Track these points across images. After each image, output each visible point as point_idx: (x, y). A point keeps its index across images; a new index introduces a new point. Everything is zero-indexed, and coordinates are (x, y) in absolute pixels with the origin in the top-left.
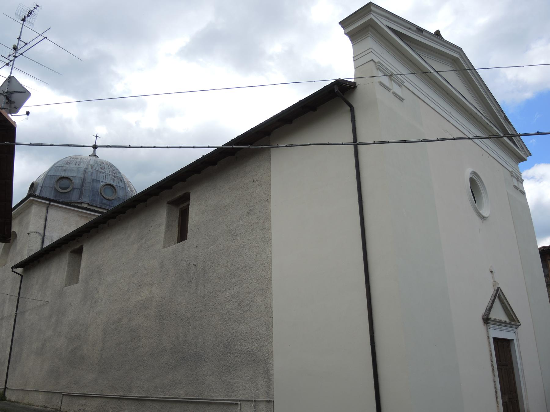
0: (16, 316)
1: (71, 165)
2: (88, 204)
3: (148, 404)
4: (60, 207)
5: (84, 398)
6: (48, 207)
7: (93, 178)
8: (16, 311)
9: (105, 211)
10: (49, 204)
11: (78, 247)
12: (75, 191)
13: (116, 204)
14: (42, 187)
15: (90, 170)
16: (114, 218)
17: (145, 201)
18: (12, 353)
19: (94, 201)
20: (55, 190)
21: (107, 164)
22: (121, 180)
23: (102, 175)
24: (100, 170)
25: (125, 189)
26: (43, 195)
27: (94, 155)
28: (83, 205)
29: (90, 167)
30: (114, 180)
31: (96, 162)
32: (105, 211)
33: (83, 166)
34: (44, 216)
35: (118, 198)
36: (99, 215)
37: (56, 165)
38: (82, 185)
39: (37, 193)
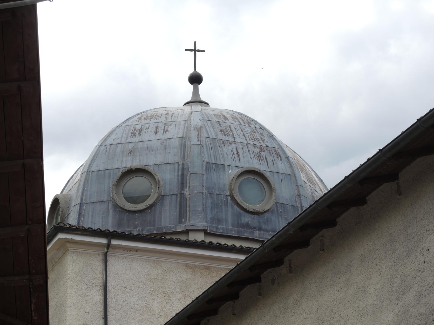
1: (145, 137)
2: (206, 233)
4: (137, 250)
6: (106, 255)
7: (206, 160)
9: (256, 246)
10: (109, 246)
12: (167, 201)
13: (280, 224)
14: (81, 204)
16: (305, 243)
17: (393, 176)
19: (219, 221)
20: (116, 206)
21: (234, 118)
22: (279, 155)
23: (228, 149)
24: (221, 136)
25: (292, 177)
26: (87, 224)
27: (196, 100)
28: (192, 237)
29: (193, 134)
30: (259, 157)
31: (206, 119)
32: (256, 246)
33: (175, 132)
35: (279, 207)
36: (242, 257)
37: (109, 142)
38: (183, 184)
39: (72, 220)
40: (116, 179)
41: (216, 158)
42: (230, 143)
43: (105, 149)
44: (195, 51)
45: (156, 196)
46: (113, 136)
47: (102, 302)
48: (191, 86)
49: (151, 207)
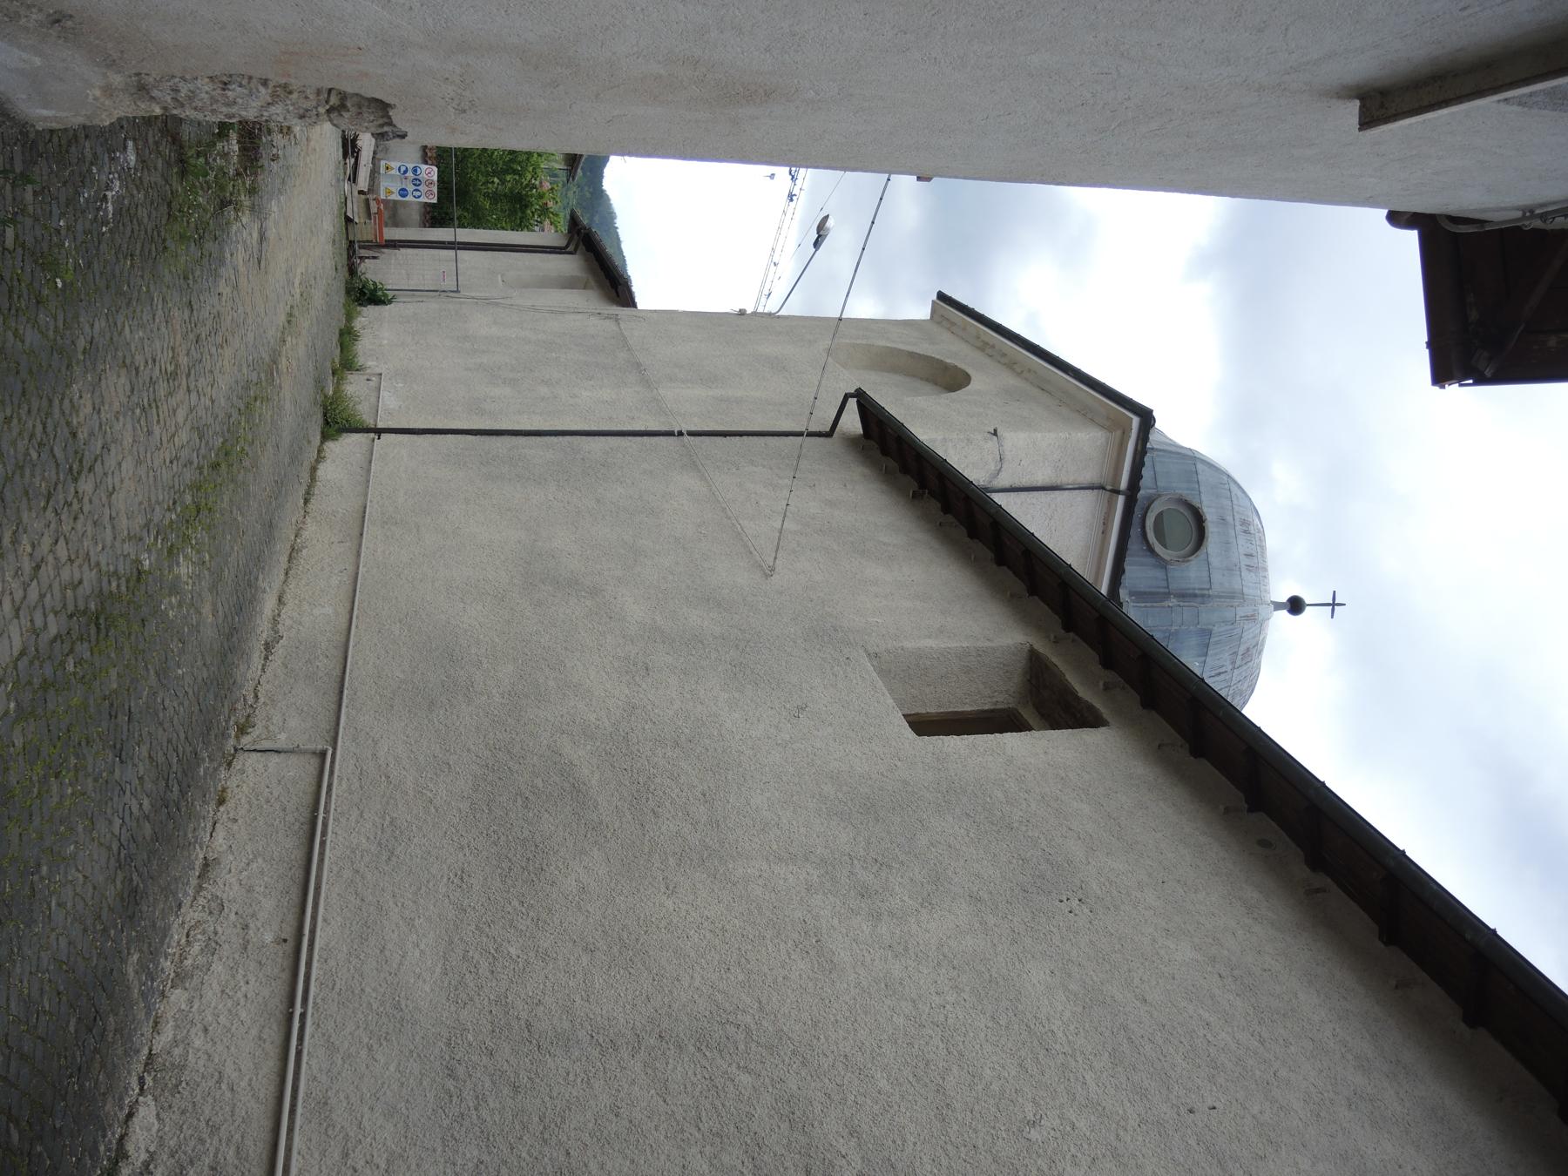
0: (670, 434)
1: (1242, 539)
3: (273, 1034)
4: (1105, 533)
5: (288, 932)
7: (1216, 629)
8: (691, 434)
10: (1117, 492)
11: (1083, 692)
12: (1159, 574)
15: (1241, 612)
18: (522, 440)
24: (1242, 649)
34: (1064, 479)
38: (1183, 596)
40: (1189, 499)
41: (1217, 643)
42: (1233, 663)
43: (1224, 482)
44: (1333, 604)
45: (1167, 558)
46: (1239, 493)
47: (1034, 484)
48: (1284, 599)
49: (1151, 550)
